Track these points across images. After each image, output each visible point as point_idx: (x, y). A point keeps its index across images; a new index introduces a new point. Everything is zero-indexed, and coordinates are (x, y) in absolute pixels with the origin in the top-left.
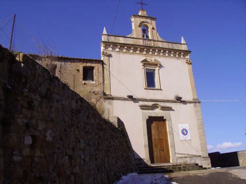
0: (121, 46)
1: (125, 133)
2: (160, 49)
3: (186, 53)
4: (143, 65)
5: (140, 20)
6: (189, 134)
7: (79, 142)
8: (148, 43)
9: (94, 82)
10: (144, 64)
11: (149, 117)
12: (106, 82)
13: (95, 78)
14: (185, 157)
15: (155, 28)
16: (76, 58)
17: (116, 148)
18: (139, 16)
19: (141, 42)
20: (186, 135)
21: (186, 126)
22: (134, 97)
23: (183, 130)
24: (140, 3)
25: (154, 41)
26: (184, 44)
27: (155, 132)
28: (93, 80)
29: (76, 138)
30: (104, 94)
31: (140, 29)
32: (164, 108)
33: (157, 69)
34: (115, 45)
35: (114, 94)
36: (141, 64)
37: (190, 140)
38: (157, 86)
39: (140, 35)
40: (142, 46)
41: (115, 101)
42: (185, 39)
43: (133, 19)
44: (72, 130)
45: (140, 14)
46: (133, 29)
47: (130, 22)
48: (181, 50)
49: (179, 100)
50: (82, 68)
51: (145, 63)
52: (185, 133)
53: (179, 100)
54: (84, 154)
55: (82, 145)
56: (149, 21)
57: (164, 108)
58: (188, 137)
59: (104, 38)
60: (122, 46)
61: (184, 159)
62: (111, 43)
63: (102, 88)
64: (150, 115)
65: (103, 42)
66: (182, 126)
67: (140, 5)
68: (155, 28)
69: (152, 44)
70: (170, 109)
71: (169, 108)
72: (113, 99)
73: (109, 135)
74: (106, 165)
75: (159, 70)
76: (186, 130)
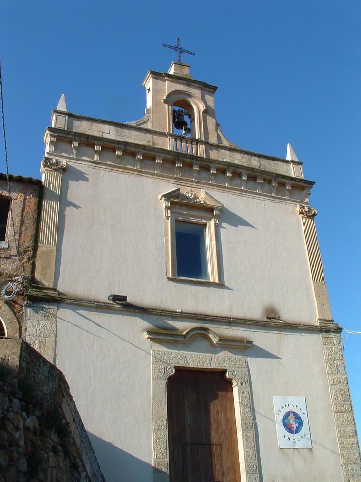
0: (103, 148)
2: (223, 169)
3: (301, 186)
4: (167, 208)
5: (168, 87)
6: (279, 418)
8: (187, 148)
10: (173, 203)
11: (178, 369)
12: (41, 249)
15: (147, 91)
18: (169, 76)
19: (168, 144)
20: (297, 431)
21: (296, 403)
22: (129, 300)
23: (287, 415)
24: (176, 48)
25: (206, 143)
26: (294, 162)
30: (32, 281)
31: (167, 110)
32: (227, 343)
33: (211, 225)
34: (88, 141)
36: (164, 204)
37: (311, 449)
38: (212, 275)
39: (167, 125)
40: (169, 152)
41: (65, 313)
42: (295, 149)
43: (149, 83)
45: (172, 71)
46: (148, 107)
47: (143, 92)
48: (284, 177)
51: (175, 200)
56: (197, 92)
57: (227, 343)
58: (300, 441)
59: (55, 121)
60: (109, 146)
62: (76, 134)
63: (28, 267)
64: (181, 364)
65: (51, 129)
67: (175, 53)
68: (147, 91)
69: (201, 151)
70: (245, 347)
71: (241, 341)
72: (58, 300)
75: (217, 227)
76: (297, 417)
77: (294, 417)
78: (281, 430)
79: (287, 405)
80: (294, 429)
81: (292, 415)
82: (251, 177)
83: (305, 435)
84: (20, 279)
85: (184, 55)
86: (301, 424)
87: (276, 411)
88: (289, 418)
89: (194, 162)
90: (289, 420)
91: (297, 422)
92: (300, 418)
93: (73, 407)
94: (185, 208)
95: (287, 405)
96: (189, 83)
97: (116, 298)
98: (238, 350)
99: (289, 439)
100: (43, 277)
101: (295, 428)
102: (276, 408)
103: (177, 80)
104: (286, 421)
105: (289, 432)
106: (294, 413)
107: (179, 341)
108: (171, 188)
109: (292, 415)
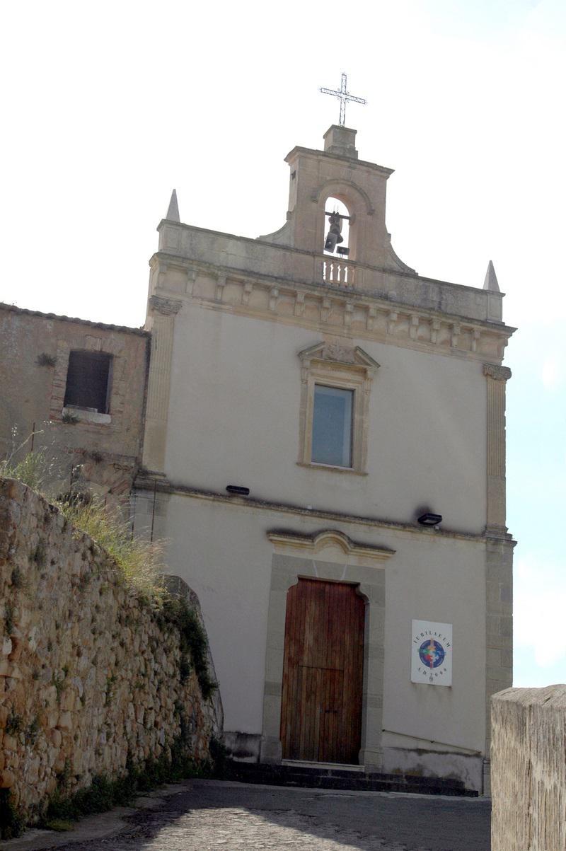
1: (490, 282)
6: (448, 662)
7: (79, 654)
9: (105, 419)
11: (301, 579)
13: (115, 402)
14: (420, 752)
16: (46, 311)
17: (161, 682)
20: (437, 664)
21: (443, 633)
23: (427, 644)
27: (316, 640)
28: (103, 409)
29: (74, 646)
30: (144, 473)
35: (174, 467)
41: (177, 500)
44: (70, 625)
49: (427, 519)
50: (67, 357)
52: (434, 658)
53: (427, 519)
54: (83, 685)
55: (84, 663)
58: (443, 675)
61: (414, 755)
64: (307, 573)
66: (423, 630)
72: (171, 488)
73: (145, 638)
74: (129, 725)
76: (439, 648)
77: (435, 647)
78: (416, 660)
79: (428, 633)
80: (432, 663)
81: (432, 645)
82: (423, 320)
83: (445, 670)
84: (100, 489)
85: (351, 105)
86: (442, 657)
87: (414, 638)
88: (429, 647)
89: (348, 300)
90: (428, 650)
91: (437, 654)
92: (442, 650)
93: (323, 516)
94: (329, 368)
95: (428, 633)
96: (353, 165)
97: (229, 488)
98: (376, 560)
99: (425, 673)
100: (149, 464)
101: (434, 661)
102: (415, 633)
103: (335, 161)
104: (424, 651)
105: (426, 665)
106: (436, 643)
107: (305, 545)
108: (307, 336)
109: (432, 645)
